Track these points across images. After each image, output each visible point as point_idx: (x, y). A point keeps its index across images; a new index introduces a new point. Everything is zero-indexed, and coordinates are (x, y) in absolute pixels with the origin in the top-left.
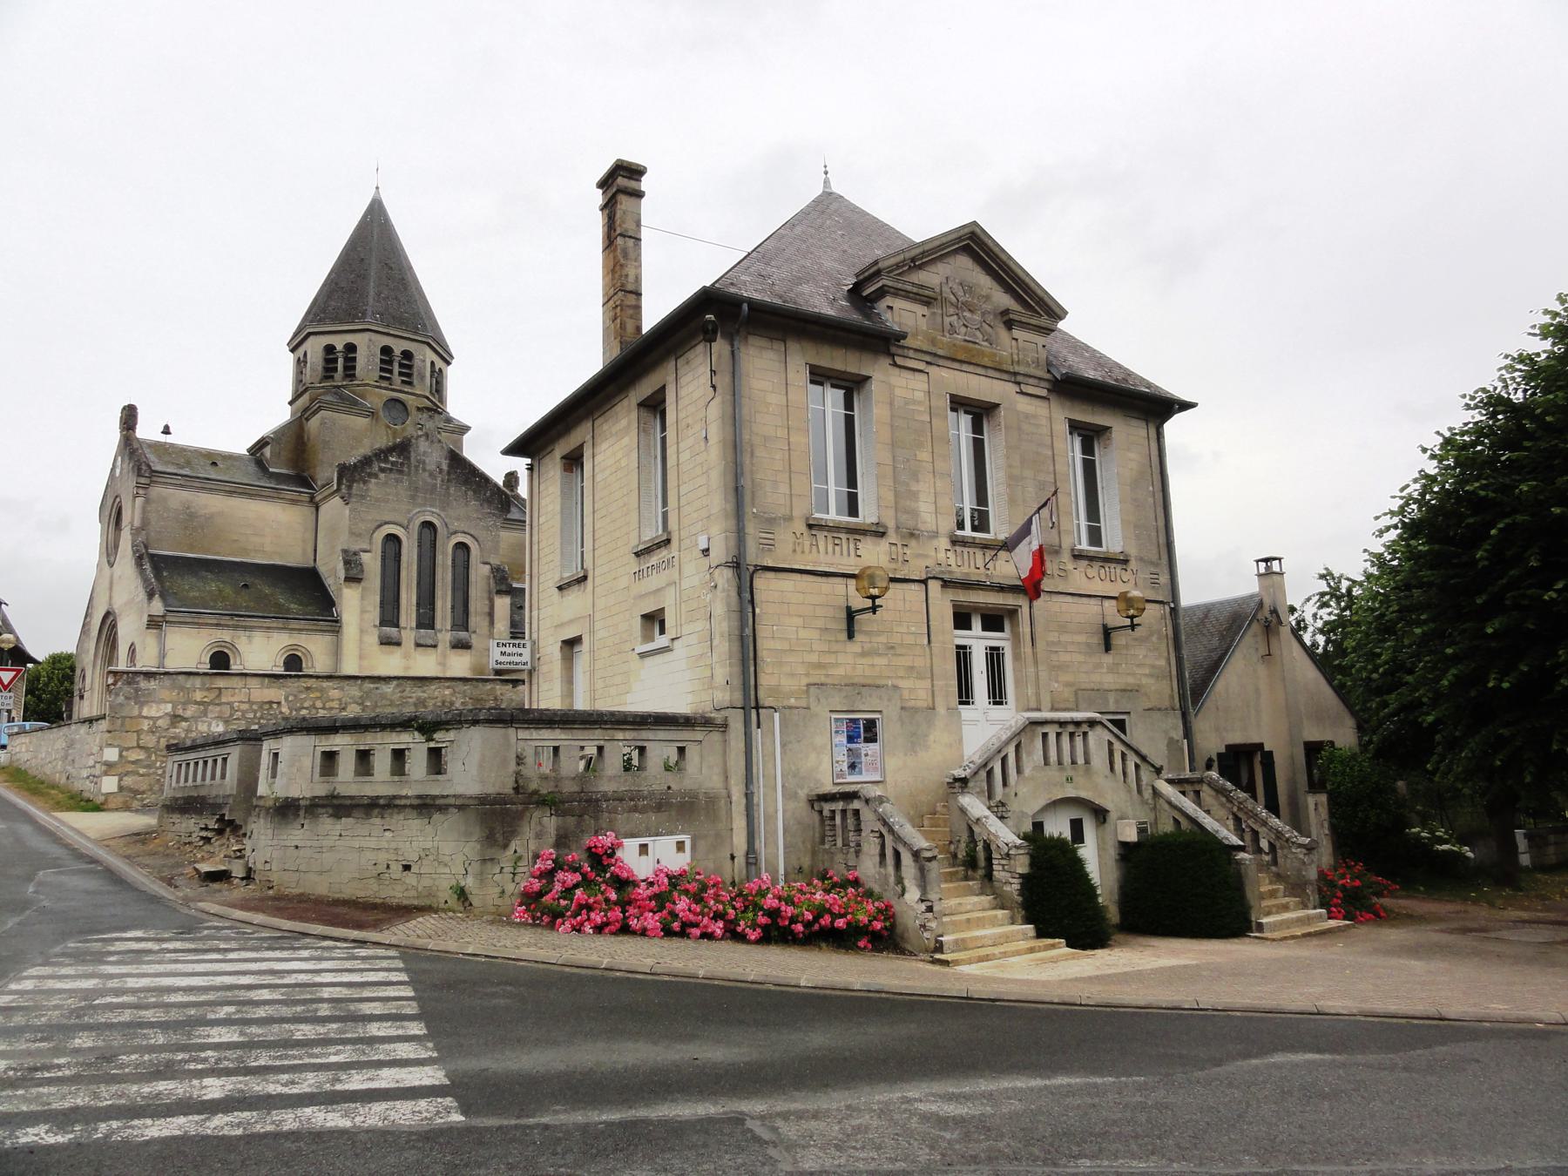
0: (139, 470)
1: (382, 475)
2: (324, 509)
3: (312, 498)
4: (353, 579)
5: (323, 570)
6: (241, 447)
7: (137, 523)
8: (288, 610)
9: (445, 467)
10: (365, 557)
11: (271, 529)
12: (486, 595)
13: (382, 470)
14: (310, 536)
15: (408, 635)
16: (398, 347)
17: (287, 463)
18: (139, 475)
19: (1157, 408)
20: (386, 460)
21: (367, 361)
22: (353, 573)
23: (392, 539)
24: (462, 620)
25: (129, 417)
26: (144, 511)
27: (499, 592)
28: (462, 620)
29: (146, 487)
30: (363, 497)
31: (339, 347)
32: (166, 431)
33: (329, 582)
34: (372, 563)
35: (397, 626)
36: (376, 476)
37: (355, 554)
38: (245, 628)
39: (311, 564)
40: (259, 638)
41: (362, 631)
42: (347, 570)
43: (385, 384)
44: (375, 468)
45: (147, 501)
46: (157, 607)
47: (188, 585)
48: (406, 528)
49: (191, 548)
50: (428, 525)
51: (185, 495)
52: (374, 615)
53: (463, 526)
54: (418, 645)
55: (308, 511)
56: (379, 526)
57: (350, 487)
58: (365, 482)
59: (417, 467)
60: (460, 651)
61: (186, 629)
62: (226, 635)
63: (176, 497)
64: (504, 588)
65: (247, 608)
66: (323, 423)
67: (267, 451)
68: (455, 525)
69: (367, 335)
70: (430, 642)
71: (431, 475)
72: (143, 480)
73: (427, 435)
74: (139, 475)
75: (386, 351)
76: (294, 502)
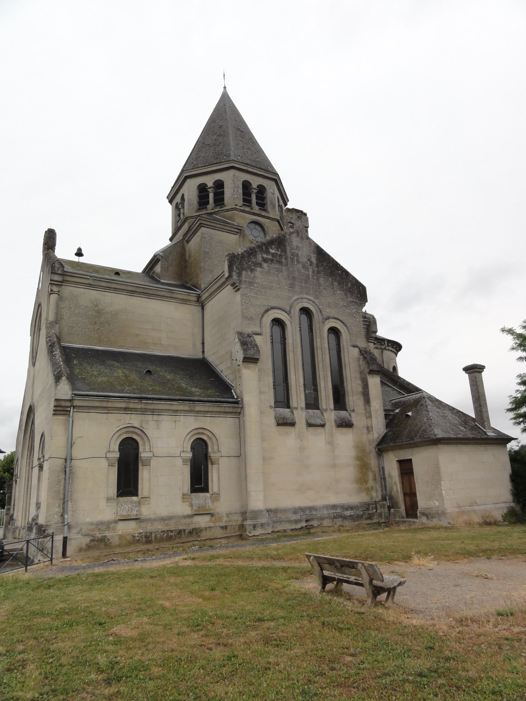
0: (53, 267)
1: (265, 265)
2: (208, 307)
3: (199, 297)
4: (251, 360)
5: (212, 358)
6: (138, 266)
7: (51, 318)
8: (191, 394)
9: (314, 261)
10: (258, 339)
11: (167, 327)
12: (358, 375)
13: (265, 260)
14: (198, 330)
15: (300, 415)
16: (255, 182)
17: (175, 272)
18: (53, 273)
19: (278, 425)
20: (267, 252)
21: (232, 194)
22: (251, 353)
23: (278, 322)
24: (340, 400)
25: (50, 239)
26: (57, 306)
27: (372, 372)
28: (340, 400)
29: (60, 284)
30: (251, 283)
31: (210, 184)
32: (79, 253)
33: (223, 369)
34: (264, 343)
35: (288, 407)
36: (260, 265)
37: (249, 336)
38: (153, 412)
39: (200, 356)
40: (166, 421)
41: (262, 413)
42: (245, 350)
43: (247, 209)
44: (259, 258)
45: (61, 298)
46: (65, 390)
47: (97, 373)
48: (289, 313)
49: (99, 343)
50: (305, 311)
51: (94, 294)
52: (270, 397)
53: (333, 312)
54: (310, 425)
55: (195, 309)
56: (267, 311)
57: (240, 275)
58: (252, 270)
59: (292, 259)
60: (344, 430)
61: (94, 415)
62: (135, 420)
63: (87, 296)
64: (375, 367)
65: (154, 392)
66: (203, 238)
67: (158, 269)
68: (327, 312)
69: (232, 172)
70: (319, 422)
71: (304, 267)
72: (56, 278)
73: (298, 233)
74: (53, 273)
75: (246, 185)
76: (184, 302)
